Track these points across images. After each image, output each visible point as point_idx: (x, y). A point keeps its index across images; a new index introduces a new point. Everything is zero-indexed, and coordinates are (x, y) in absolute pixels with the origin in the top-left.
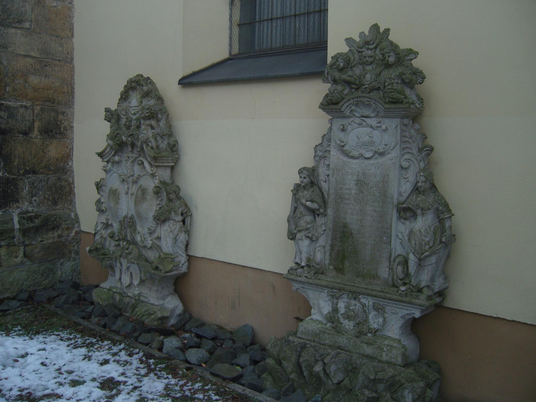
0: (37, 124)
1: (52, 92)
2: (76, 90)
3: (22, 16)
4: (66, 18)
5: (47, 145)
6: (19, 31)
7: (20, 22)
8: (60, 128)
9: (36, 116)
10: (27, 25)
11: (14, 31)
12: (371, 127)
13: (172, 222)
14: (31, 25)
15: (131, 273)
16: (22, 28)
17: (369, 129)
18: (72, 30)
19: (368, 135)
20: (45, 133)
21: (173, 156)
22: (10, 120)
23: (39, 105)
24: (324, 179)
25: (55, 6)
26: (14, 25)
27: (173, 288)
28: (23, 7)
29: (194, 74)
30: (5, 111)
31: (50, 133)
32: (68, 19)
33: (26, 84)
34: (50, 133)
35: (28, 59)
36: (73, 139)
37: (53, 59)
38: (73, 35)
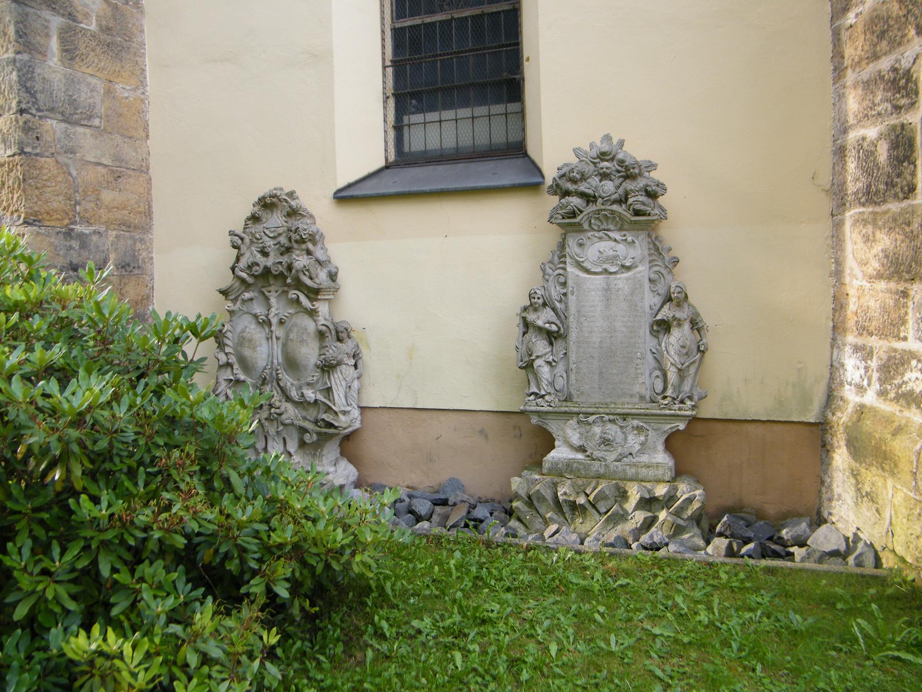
0: (112, 256)
1: (128, 212)
2: (154, 209)
3: (90, 110)
4: (139, 113)
5: (125, 284)
6: (88, 131)
7: (90, 117)
8: (138, 260)
9: (112, 245)
10: (96, 122)
11: (81, 130)
12: (615, 240)
13: (344, 366)
14: (100, 122)
15: (284, 439)
16: (90, 126)
17: (613, 244)
18: (146, 128)
19: (612, 248)
20: (123, 267)
21: (15, 317)
22: (82, 252)
23: (115, 229)
24: (559, 299)
25: (127, 98)
26: (82, 123)
27: (339, 451)
28: (90, 98)
29: (350, 186)
30: (76, 240)
31: (127, 268)
32: (141, 115)
33: (98, 202)
34: (127, 268)
35: (100, 169)
36: (152, 274)
37: (127, 168)
38: (147, 136)
